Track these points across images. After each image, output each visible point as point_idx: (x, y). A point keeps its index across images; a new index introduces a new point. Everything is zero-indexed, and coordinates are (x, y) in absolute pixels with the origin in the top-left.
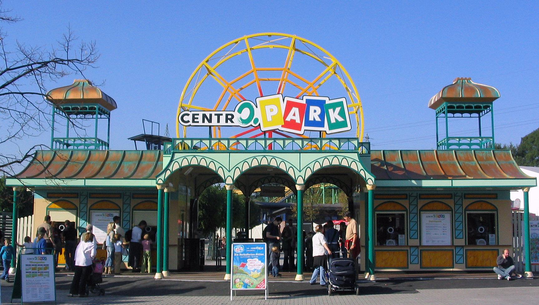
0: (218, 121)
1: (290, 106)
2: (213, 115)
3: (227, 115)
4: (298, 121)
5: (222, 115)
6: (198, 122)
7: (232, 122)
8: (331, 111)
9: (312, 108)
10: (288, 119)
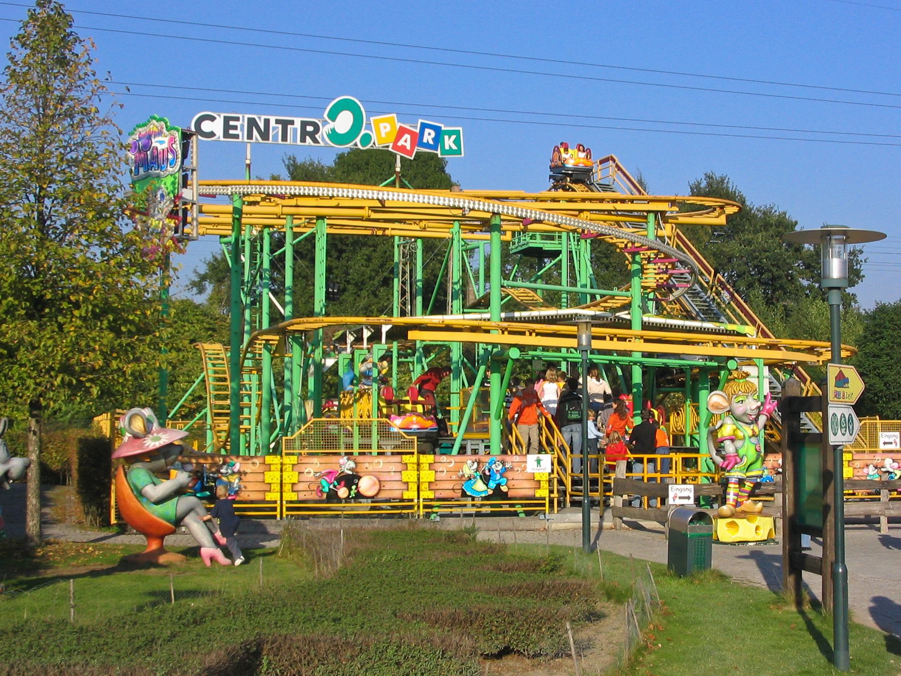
0: (284, 138)
1: (402, 132)
2: (272, 124)
3: (304, 124)
4: (408, 147)
5: (292, 123)
6: (237, 136)
7: (315, 141)
8: (446, 137)
9: (427, 131)
10: (399, 144)
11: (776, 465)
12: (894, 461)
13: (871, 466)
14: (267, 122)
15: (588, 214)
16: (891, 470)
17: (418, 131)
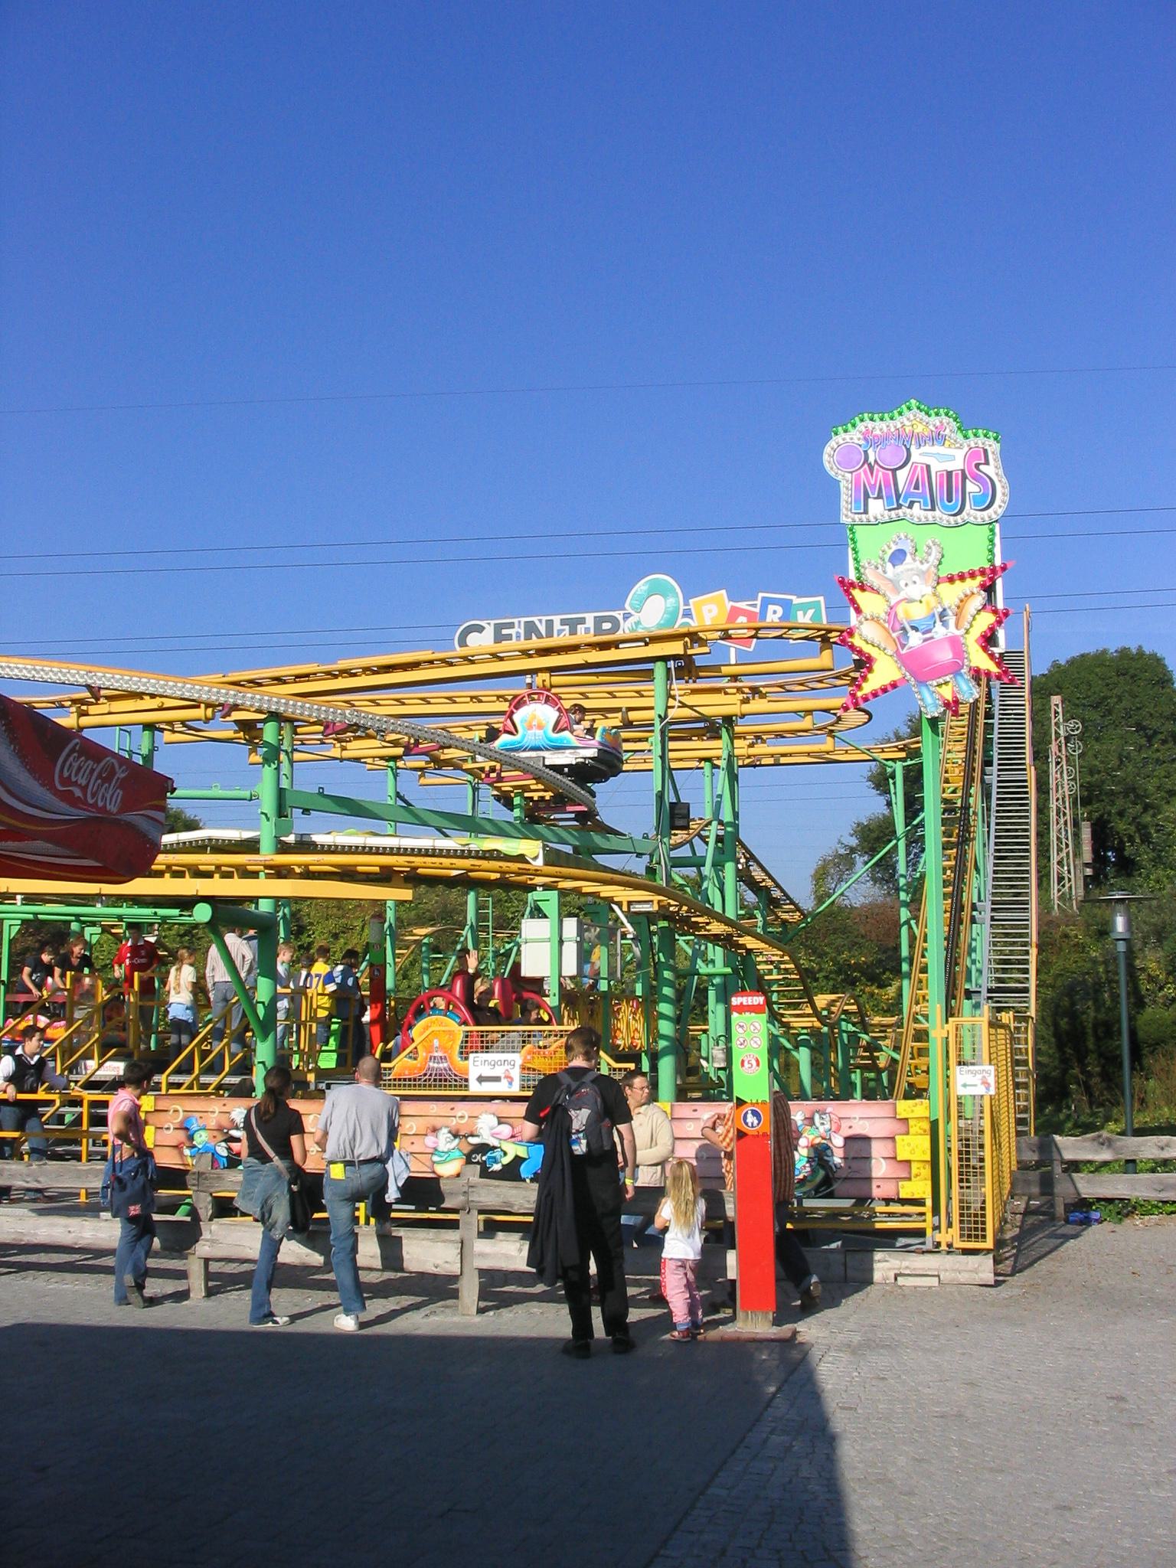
1: (734, 613)
2: (557, 626)
5: (582, 621)
9: (771, 608)
11: (225, 1123)
12: (501, 1121)
13: (445, 1131)
14: (550, 624)
15: (545, 676)
16: (493, 1142)
17: (757, 610)
